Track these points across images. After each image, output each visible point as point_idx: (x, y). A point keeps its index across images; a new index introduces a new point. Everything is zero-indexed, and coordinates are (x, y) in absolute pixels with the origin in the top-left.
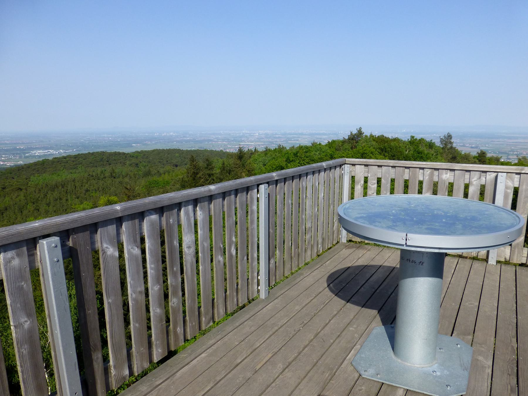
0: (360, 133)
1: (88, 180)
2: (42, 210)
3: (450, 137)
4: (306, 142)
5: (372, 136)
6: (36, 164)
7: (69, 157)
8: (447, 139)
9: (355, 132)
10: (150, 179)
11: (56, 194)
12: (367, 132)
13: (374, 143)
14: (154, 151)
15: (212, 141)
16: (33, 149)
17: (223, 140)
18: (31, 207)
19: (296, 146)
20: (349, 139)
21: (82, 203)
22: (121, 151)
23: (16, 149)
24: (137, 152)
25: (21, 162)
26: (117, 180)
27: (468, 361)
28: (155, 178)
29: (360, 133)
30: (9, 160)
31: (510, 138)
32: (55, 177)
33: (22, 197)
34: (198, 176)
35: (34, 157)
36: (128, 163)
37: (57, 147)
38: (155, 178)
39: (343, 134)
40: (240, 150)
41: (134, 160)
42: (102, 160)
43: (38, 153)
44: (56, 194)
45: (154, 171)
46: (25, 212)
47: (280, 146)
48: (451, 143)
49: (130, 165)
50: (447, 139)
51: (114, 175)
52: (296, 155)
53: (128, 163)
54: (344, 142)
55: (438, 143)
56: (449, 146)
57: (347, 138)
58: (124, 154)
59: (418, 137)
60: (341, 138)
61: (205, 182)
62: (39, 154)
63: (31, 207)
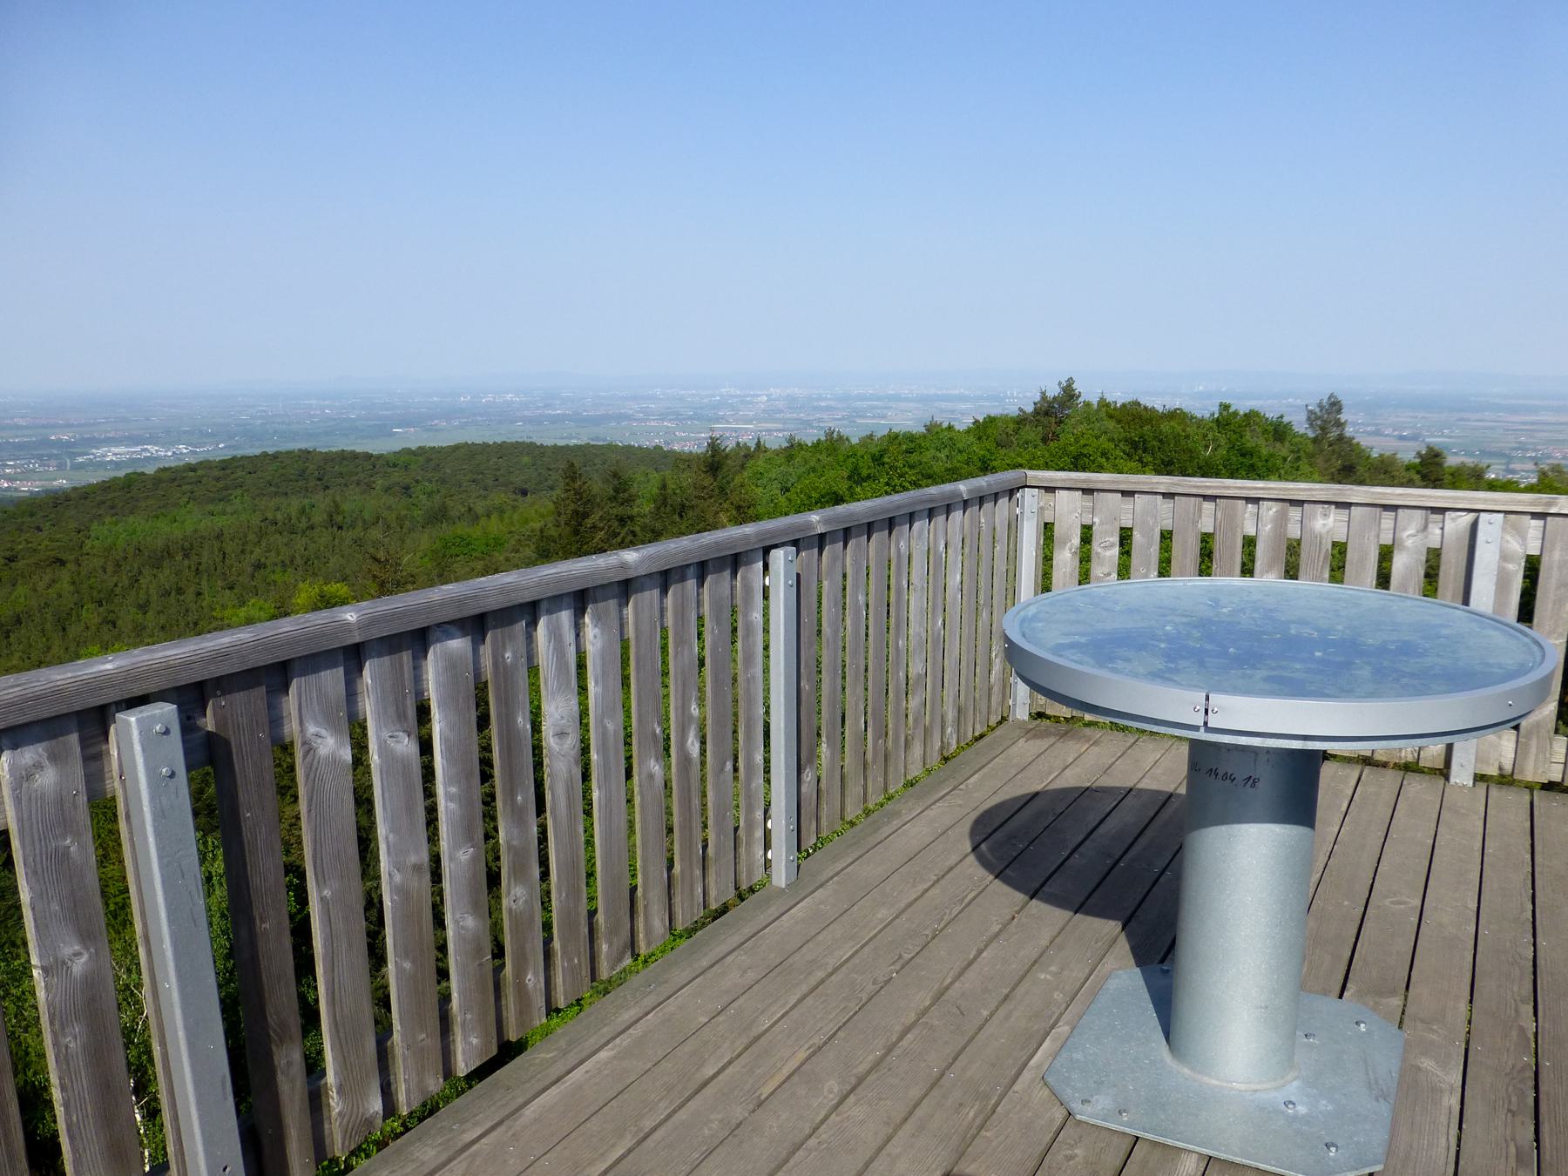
0: (1069, 394)
1: (262, 534)
2: (125, 623)
3: (1335, 405)
4: (909, 421)
5: (1103, 403)
6: (106, 487)
7: (205, 465)
8: (1329, 414)
9: (1054, 391)
10: (446, 530)
11: (166, 576)
12: (1089, 392)
13: (1111, 424)
14: (456, 448)
15: (628, 418)
16: (98, 443)
17: (663, 417)
18: (91, 615)
19: (880, 434)
20: (1037, 412)
21: (243, 603)
22: (359, 449)
23: (46, 443)
24: (408, 451)
25: (62, 483)
26: (348, 535)
27: (1391, 1073)
28: (462, 529)
29: (1069, 394)
30: (26, 475)
31: (1514, 410)
32: (163, 526)
33: (65, 586)
34: (589, 522)
35: (102, 465)
36: (380, 483)
37: (168, 436)
38: (462, 529)
39: (1019, 398)
40: (714, 446)
41: (397, 476)
42: (302, 474)
43: (113, 453)
44: (166, 576)
45: (456, 509)
46: (74, 630)
47: (830, 433)
48: (1339, 424)
49: (387, 490)
50: (1329, 414)
51: (339, 519)
52: (878, 459)
53: (380, 483)
54: (1021, 421)
55: (1300, 424)
56: (1333, 434)
57: (1029, 409)
58: (368, 456)
59: (1242, 406)
60: (1013, 411)
61: (608, 539)
62: (115, 457)
63: (91, 615)
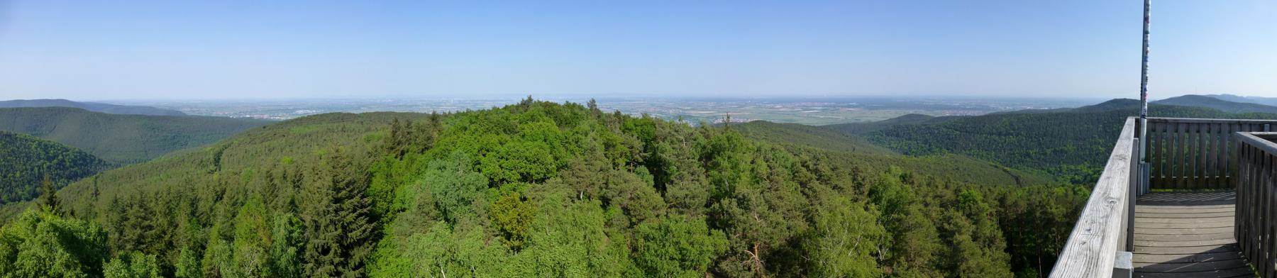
0: (530, 99)
1: (327, 132)
2: (294, 152)
3: (594, 101)
4: (488, 107)
5: (539, 102)
6: (296, 119)
7: (318, 115)
8: (592, 103)
9: (526, 98)
10: (369, 134)
11: (305, 141)
12: (535, 99)
13: (541, 107)
14: (375, 113)
15: (419, 106)
16: (297, 109)
17: (427, 105)
18: (288, 149)
19: (486, 110)
20: (522, 104)
21: (320, 149)
22: (352, 112)
23: (288, 109)
24: (363, 113)
25: (289, 118)
26: (346, 134)
27: (94, 149)
28: (373, 133)
29: (530, 99)
30: (283, 116)
31: (629, 101)
32: (307, 129)
33: (284, 141)
34: (397, 134)
35: (297, 114)
36: (356, 121)
37: (311, 108)
38: (373, 133)
39: (517, 101)
40: (434, 113)
41: (360, 119)
42: (339, 117)
43: (301, 112)
44: (305, 141)
45: (373, 128)
46: (284, 152)
47: (467, 110)
48: (595, 105)
49: (358, 122)
50: (592, 103)
51: (344, 129)
52: (477, 117)
53: (356, 121)
54: (518, 107)
55: (586, 106)
56: (594, 108)
57: (520, 103)
58: (354, 114)
59: (572, 102)
60: (516, 104)
61: (1029, 200)
62: (301, 113)
63: (288, 149)
